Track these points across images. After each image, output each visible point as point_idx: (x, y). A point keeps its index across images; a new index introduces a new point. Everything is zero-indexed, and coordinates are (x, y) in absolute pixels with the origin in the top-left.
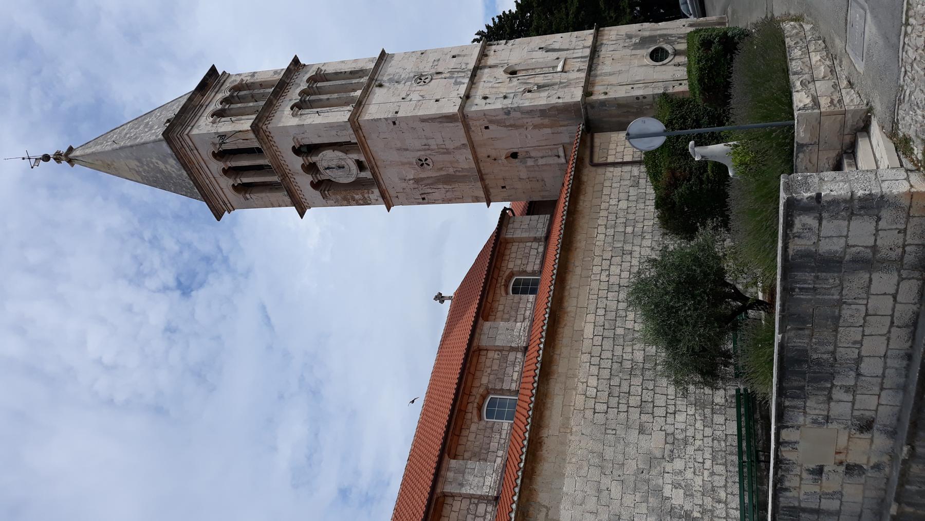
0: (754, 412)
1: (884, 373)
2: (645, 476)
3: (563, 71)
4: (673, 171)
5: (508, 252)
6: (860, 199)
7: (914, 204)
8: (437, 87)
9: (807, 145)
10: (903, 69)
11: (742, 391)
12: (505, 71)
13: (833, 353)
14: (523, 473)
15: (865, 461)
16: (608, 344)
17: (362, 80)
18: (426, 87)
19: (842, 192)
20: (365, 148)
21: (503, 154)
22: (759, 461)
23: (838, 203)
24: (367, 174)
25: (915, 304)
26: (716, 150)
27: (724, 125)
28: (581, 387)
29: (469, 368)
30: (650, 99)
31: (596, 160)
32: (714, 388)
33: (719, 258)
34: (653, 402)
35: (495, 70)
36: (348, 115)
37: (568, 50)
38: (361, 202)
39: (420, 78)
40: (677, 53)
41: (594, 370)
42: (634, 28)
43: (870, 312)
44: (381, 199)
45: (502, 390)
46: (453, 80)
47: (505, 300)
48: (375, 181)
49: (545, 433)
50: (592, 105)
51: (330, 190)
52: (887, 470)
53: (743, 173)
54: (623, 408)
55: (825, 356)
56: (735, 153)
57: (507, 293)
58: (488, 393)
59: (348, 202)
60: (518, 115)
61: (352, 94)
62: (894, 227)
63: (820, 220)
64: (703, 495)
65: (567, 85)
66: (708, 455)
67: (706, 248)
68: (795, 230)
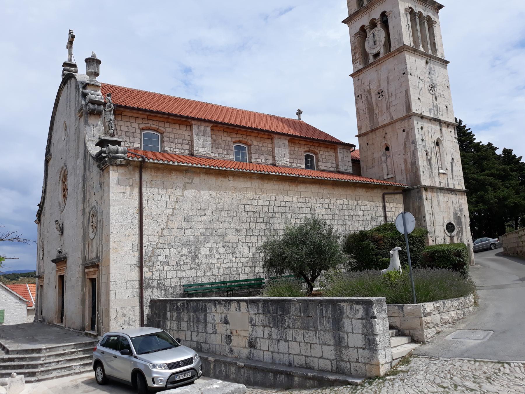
0: (252, 288)
1: (280, 353)
2: (214, 233)
3: (439, 173)
4: (382, 239)
5: (329, 150)
6: (374, 339)
7: (372, 366)
8: (428, 98)
9: (403, 311)
10: (448, 360)
11: (263, 281)
12: (438, 139)
13: (289, 327)
14: (208, 168)
15: (233, 345)
16: (281, 210)
17: (430, 51)
18: (427, 91)
19: (378, 330)
20: (388, 56)
21: (388, 143)
22: (227, 292)
23: (372, 328)
24: (371, 60)
25: (318, 368)
26: (397, 262)
27: (412, 265)
28: (257, 197)
29: (261, 134)
30: (424, 224)
31: (386, 196)
32: (263, 267)
33: (334, 266)
34: (253, 235)
35: (439, 133)
36: (408, 44)
37: (452, 175)
38: (354, 58)
39: (432, 87)
40: (452, 238)
41: (267, 203)
42: (466, 212)
43: (312, 346)
44: (356, 70)
45: (251, 153)
46: (432, 108)
47: (301, 151)
48: (367, 65)
49: (231, 179)
50: (419, 192)
51: (361, 36)
52: (230, 356)
53: (385, 277)
54: (248, 220)
55: (287, 323)
56: (396, 272)
57: (305, 152)
58: (248, 146)
59: (354, 50)
60: (412, 148)
61: (421, 45)
62: (360, 356)
63: (362, 319)
64: (207, 264)
65: (431, 176)
66: (228, 265)
67: (339, 260)
68: (354, 306)
